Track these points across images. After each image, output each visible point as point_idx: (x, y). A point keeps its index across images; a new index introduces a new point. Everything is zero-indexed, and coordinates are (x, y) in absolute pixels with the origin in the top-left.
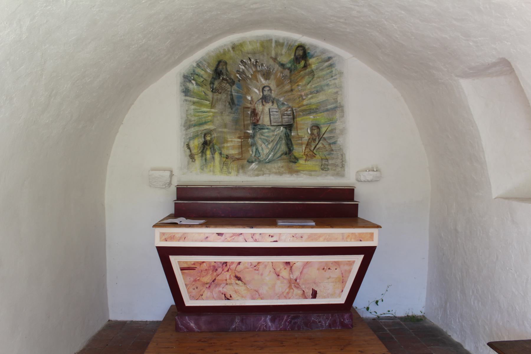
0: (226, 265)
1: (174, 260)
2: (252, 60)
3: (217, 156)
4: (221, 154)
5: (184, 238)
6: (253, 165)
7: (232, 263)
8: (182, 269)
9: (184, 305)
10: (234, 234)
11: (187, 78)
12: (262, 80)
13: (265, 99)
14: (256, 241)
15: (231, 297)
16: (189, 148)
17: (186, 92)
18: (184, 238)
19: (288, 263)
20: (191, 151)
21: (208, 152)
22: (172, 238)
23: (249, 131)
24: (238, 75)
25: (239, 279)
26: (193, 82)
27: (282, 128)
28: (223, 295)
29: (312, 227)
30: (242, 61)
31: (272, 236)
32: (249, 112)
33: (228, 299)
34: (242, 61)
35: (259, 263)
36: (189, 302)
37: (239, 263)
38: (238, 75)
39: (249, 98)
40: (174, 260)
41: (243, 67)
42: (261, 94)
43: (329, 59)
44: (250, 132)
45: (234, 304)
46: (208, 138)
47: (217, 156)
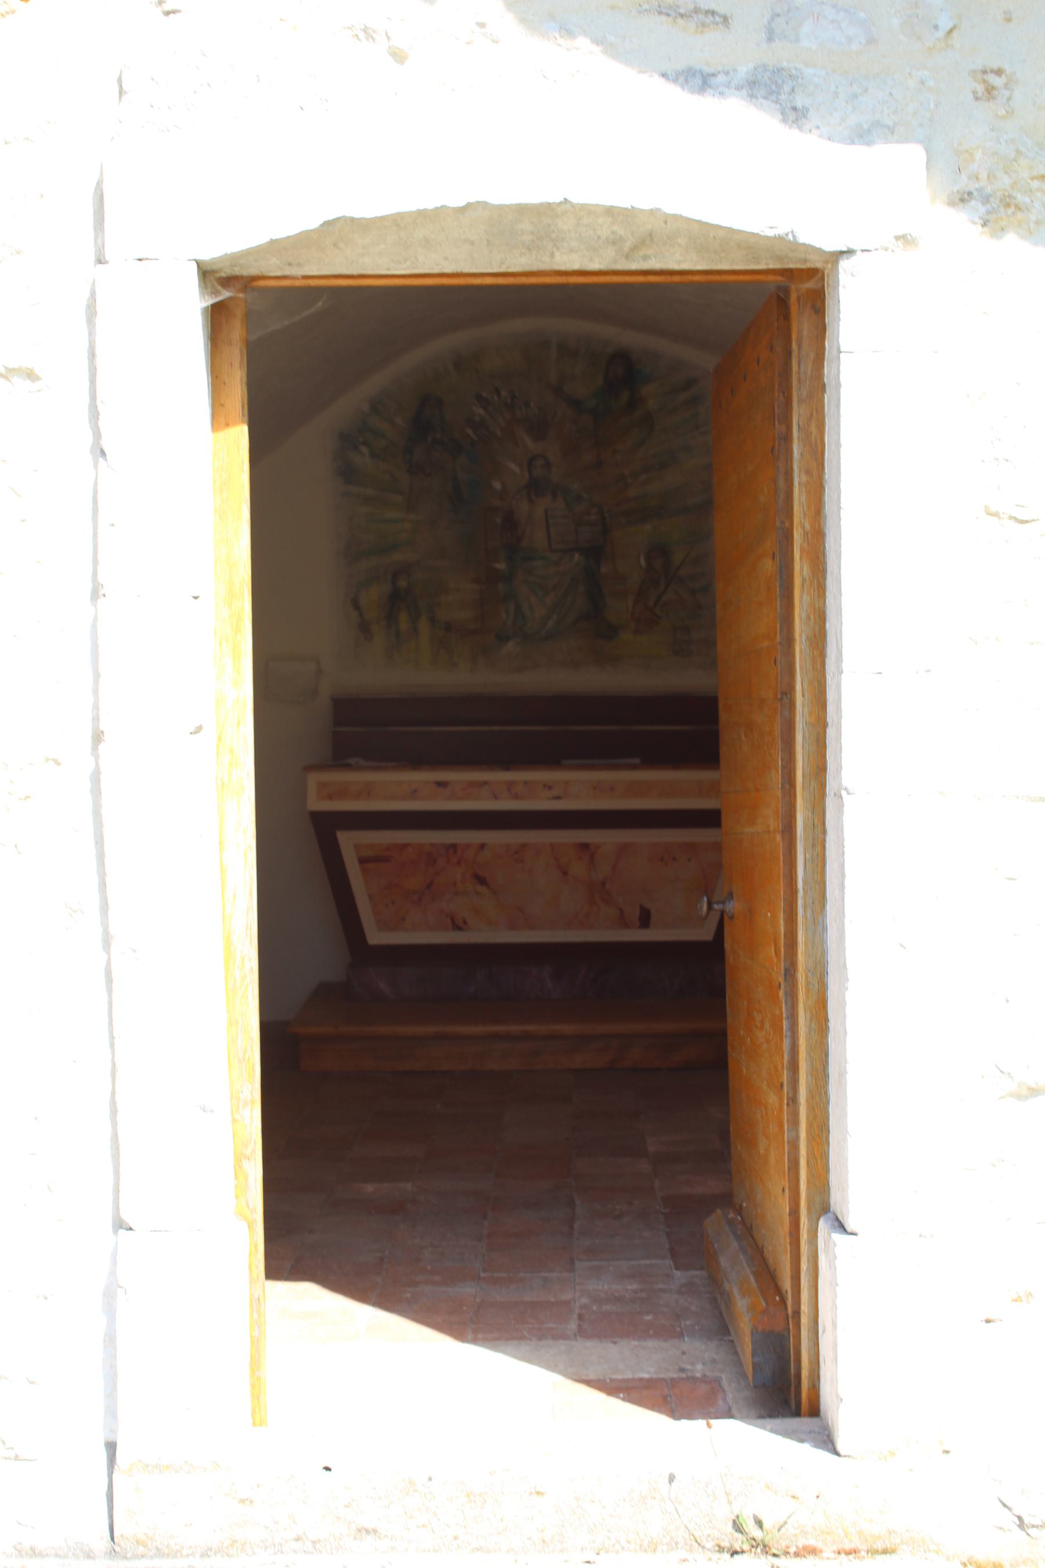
0: (455, 851)
1: (348, 841)
2: (504, 393)
3: (424, 625)
4: (433, 620)
5: (367, 791)
6: (511, 646)
7: (468, 846)
8: (362, 861)
9: (365, 940)
10: (472, 784)
11: (348, 440)
12: (529, 441)
13: (535, 488)
14: (516, 797)
15: (465, 922)
16: (356, 604)
17: (348, 473)
18: (367, 791)
19: (584, 847)
20: (361, 615)
21: (403, 618)
22: (342, 792)
23: (498, 566)
24: (469, 431)
25: (481, 881)
26: (364, 449)
27: (576, 556)
28: (449, 921)
29: (633, 767)
30: (479, 398)
31: (550, 788)
32: (498, 520)
33: (459, 929)
34: (479, 398)
35: (524, 846)
36: (375, 937)
37: (482, 846)
38: (469, 431)
39: (497, 485)
40: (348, 841)
41: (482, 411)
42: (527, 475)
43: (690, 383)
44: (501, 566)
45: (472, 940)
46: (402, 583)
47: (424, 625)
